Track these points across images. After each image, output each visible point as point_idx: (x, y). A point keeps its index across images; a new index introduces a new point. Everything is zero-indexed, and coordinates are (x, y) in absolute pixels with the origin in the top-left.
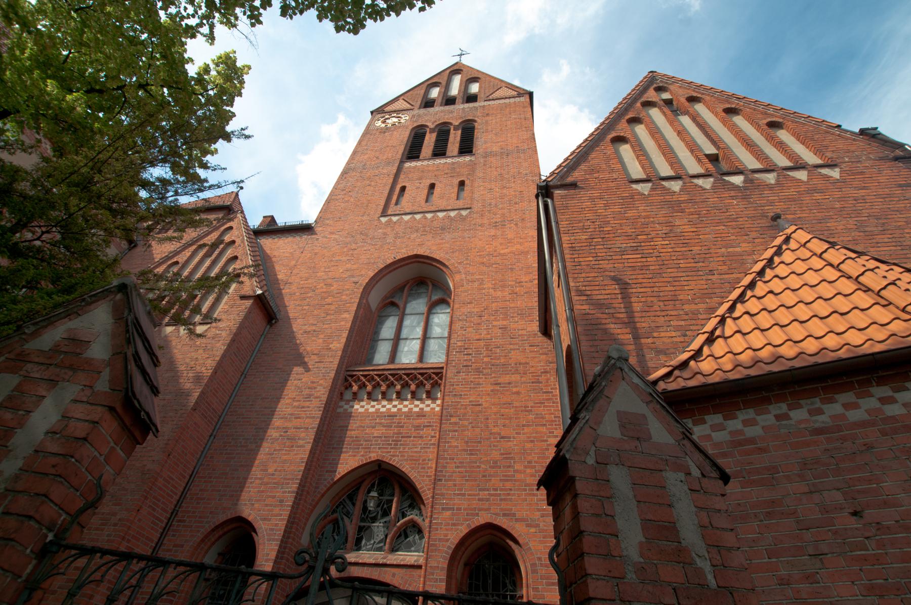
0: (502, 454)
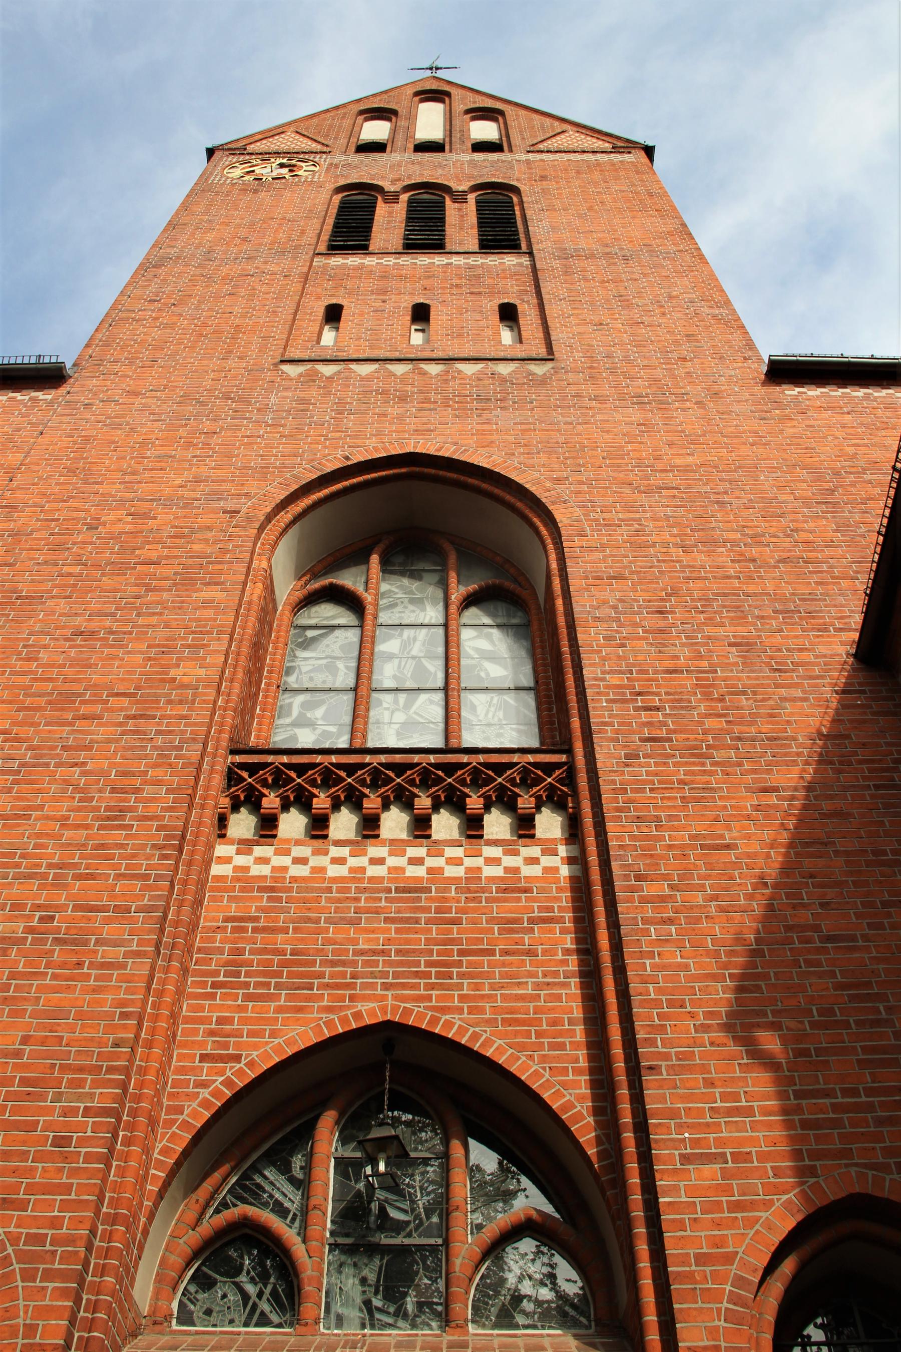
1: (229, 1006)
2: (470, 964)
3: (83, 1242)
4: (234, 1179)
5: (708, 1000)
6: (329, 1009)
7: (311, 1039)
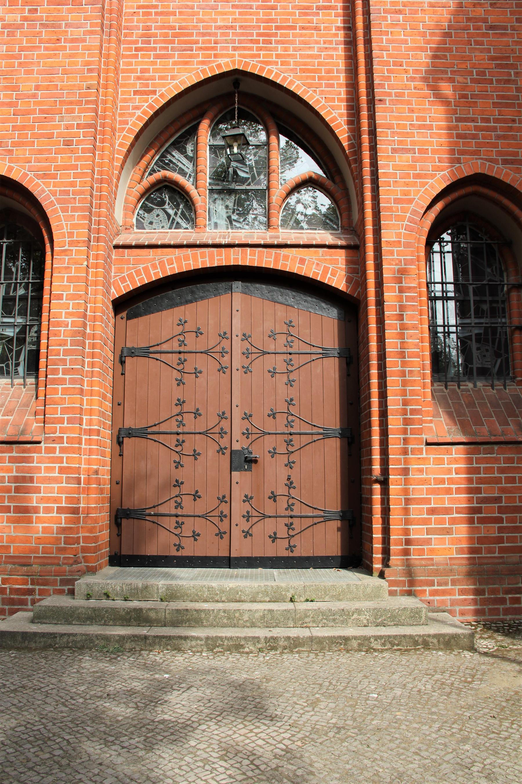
0: (492, 58)
1: (147, 62)
2: (282, 35)
3: (89, 193)
4: (157, 157)
5: (416, 63)
6: (203, 63)
7: (194, 80)
